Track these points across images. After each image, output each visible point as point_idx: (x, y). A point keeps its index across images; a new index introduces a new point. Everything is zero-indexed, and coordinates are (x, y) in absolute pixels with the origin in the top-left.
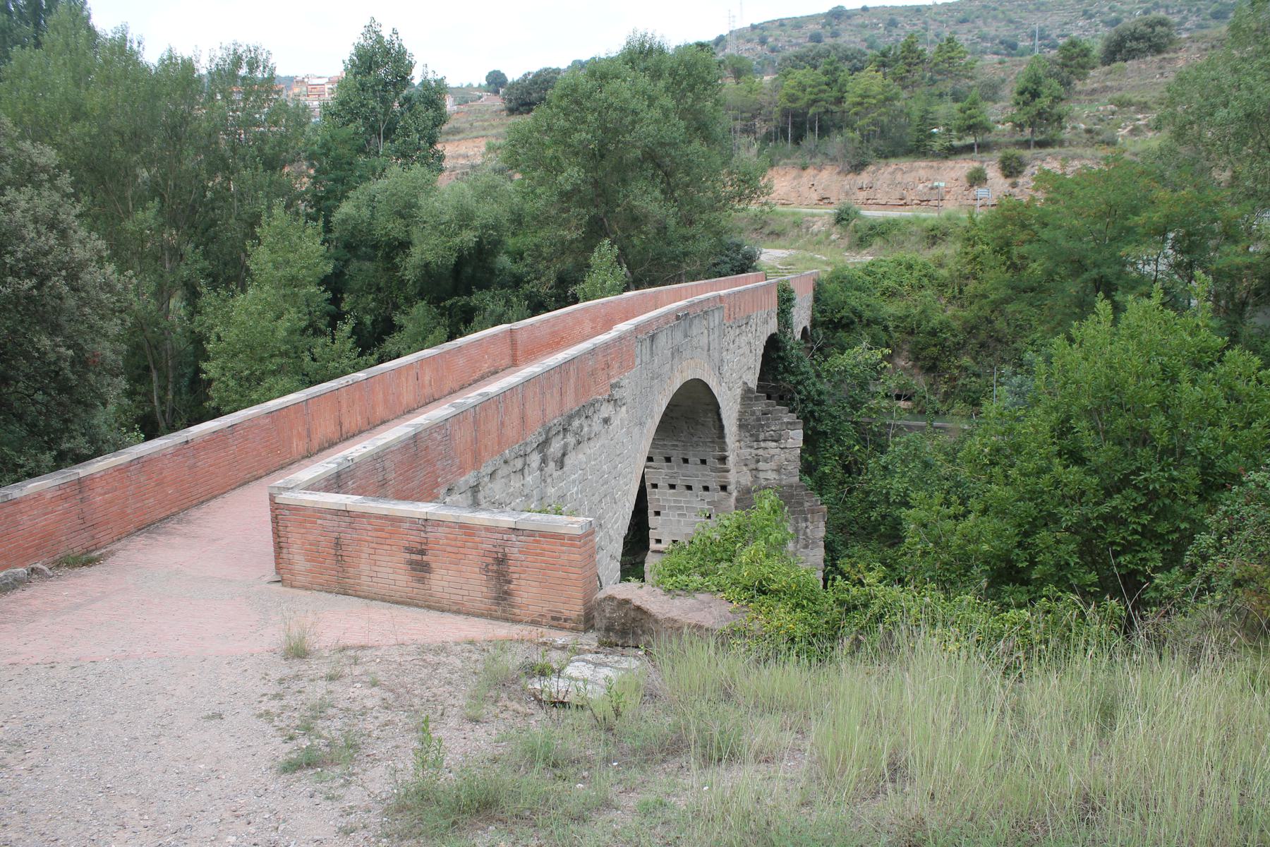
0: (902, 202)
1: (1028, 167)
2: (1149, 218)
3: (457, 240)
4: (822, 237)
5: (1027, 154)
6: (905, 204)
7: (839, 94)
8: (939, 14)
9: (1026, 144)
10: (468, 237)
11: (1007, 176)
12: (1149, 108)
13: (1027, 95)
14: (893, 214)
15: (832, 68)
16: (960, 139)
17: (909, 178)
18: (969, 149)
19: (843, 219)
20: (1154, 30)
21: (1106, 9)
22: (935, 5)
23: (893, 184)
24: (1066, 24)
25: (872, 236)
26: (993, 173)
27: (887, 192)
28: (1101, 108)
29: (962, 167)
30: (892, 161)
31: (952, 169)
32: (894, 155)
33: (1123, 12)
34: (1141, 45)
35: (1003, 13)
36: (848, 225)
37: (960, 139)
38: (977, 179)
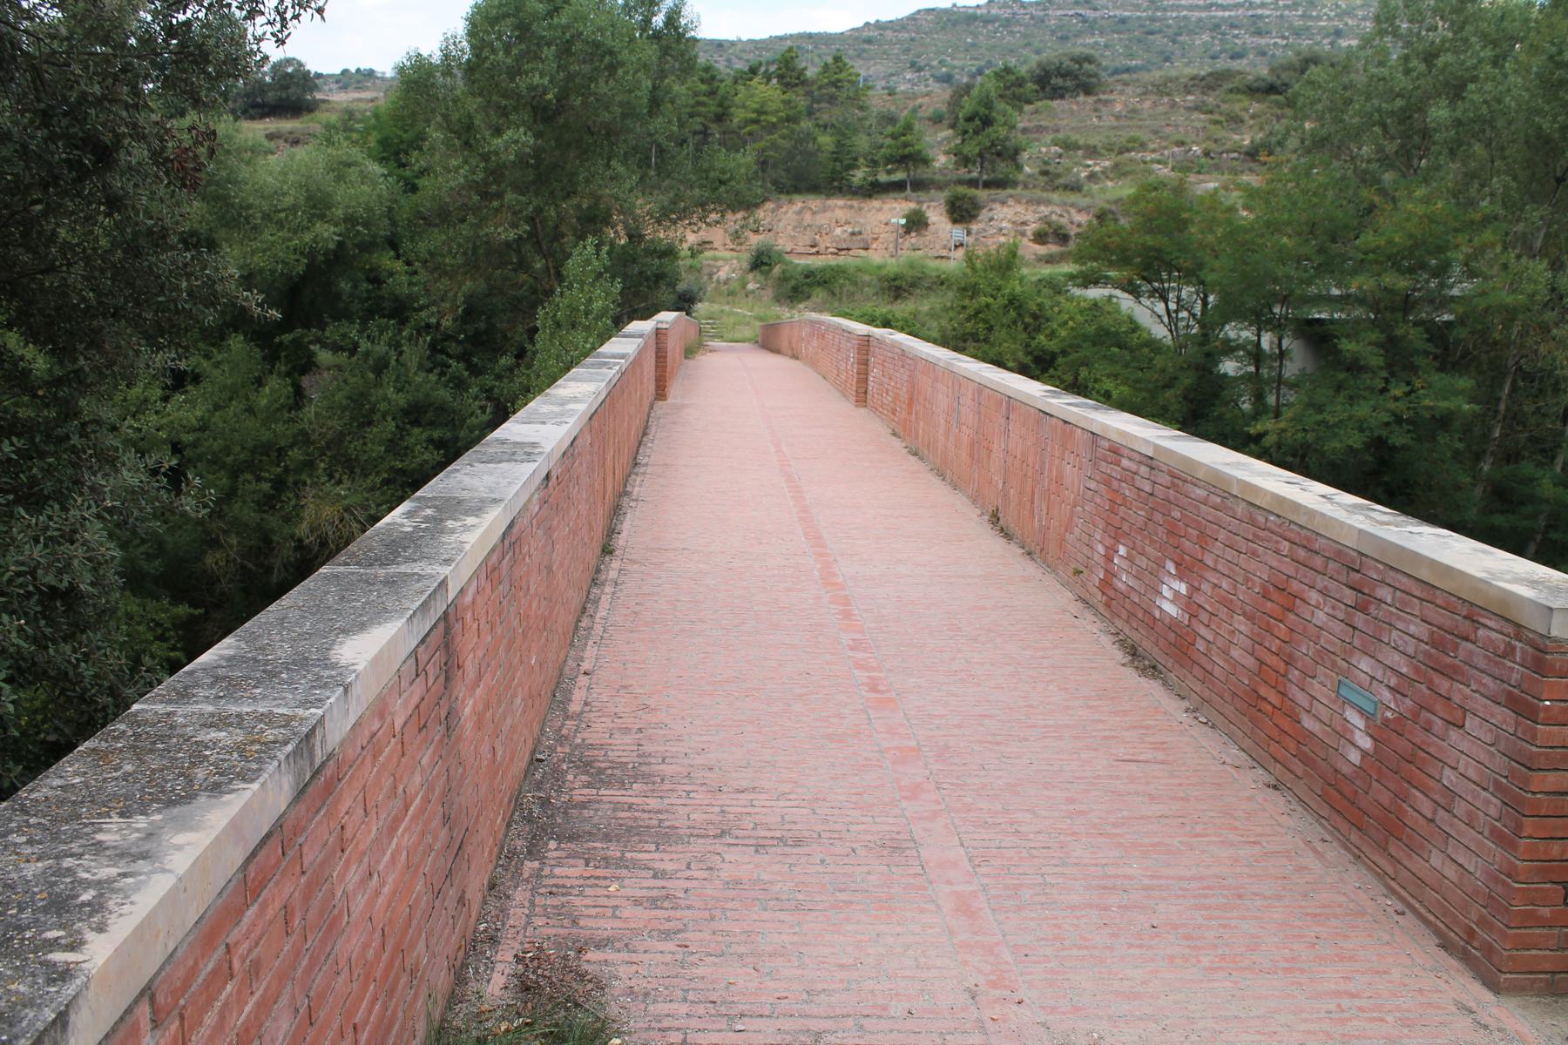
0: (814, 250)
1: (984, 211)
2: (45, 442)
3: (308, 237)
4: (734, 286)
5: (982, 194)
6: (818, 253)
7: (720, 110)
8: (745, 51)
9: (973, 183)
10: (327, 233)
11: (955, 221)
12: (1099, 154)
13: (977, 122)
14: (832, 261)
15: (708, 76)
16: (889, 172)
17: (822, 219)
18: (899, 187)
19: (763, 263)
20: (1081, 67)
21: (935, 63)
22: (740, 41)
23: (800, 227)
24: (892, 75)
25: (810, 285)
26: (937, 216)
27: (793, 238)
28: (1044, 150)
29: (894, 211)
30: (796, 197)
31: (880, 210)
32: (797, 190)
33: (954, 67)
34: (1069, 84)
35: (819, 56)
36: (771, 270)
37: (889, 172)
38: (916, 223)
